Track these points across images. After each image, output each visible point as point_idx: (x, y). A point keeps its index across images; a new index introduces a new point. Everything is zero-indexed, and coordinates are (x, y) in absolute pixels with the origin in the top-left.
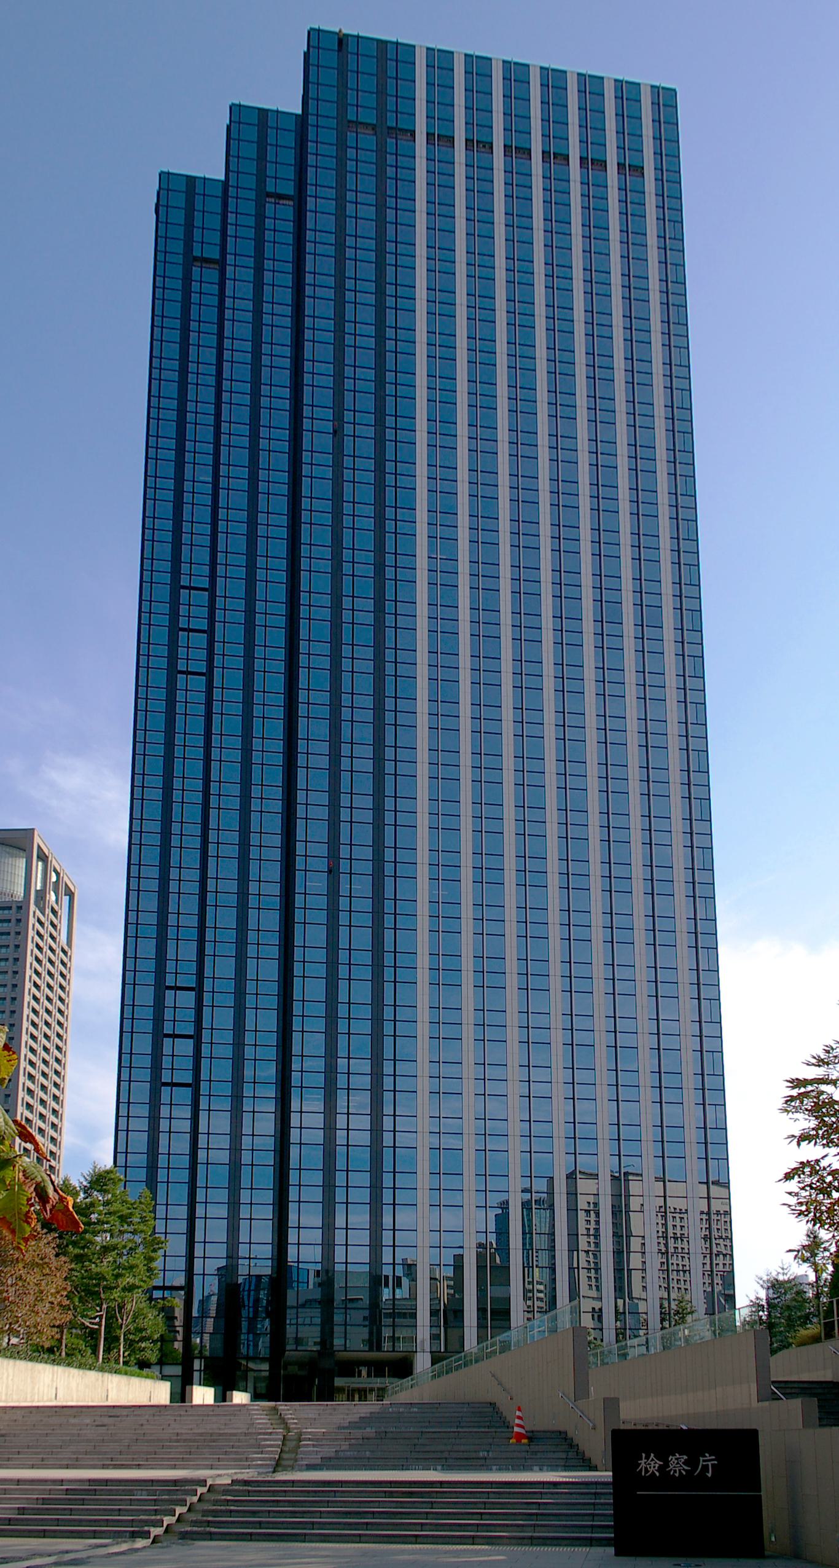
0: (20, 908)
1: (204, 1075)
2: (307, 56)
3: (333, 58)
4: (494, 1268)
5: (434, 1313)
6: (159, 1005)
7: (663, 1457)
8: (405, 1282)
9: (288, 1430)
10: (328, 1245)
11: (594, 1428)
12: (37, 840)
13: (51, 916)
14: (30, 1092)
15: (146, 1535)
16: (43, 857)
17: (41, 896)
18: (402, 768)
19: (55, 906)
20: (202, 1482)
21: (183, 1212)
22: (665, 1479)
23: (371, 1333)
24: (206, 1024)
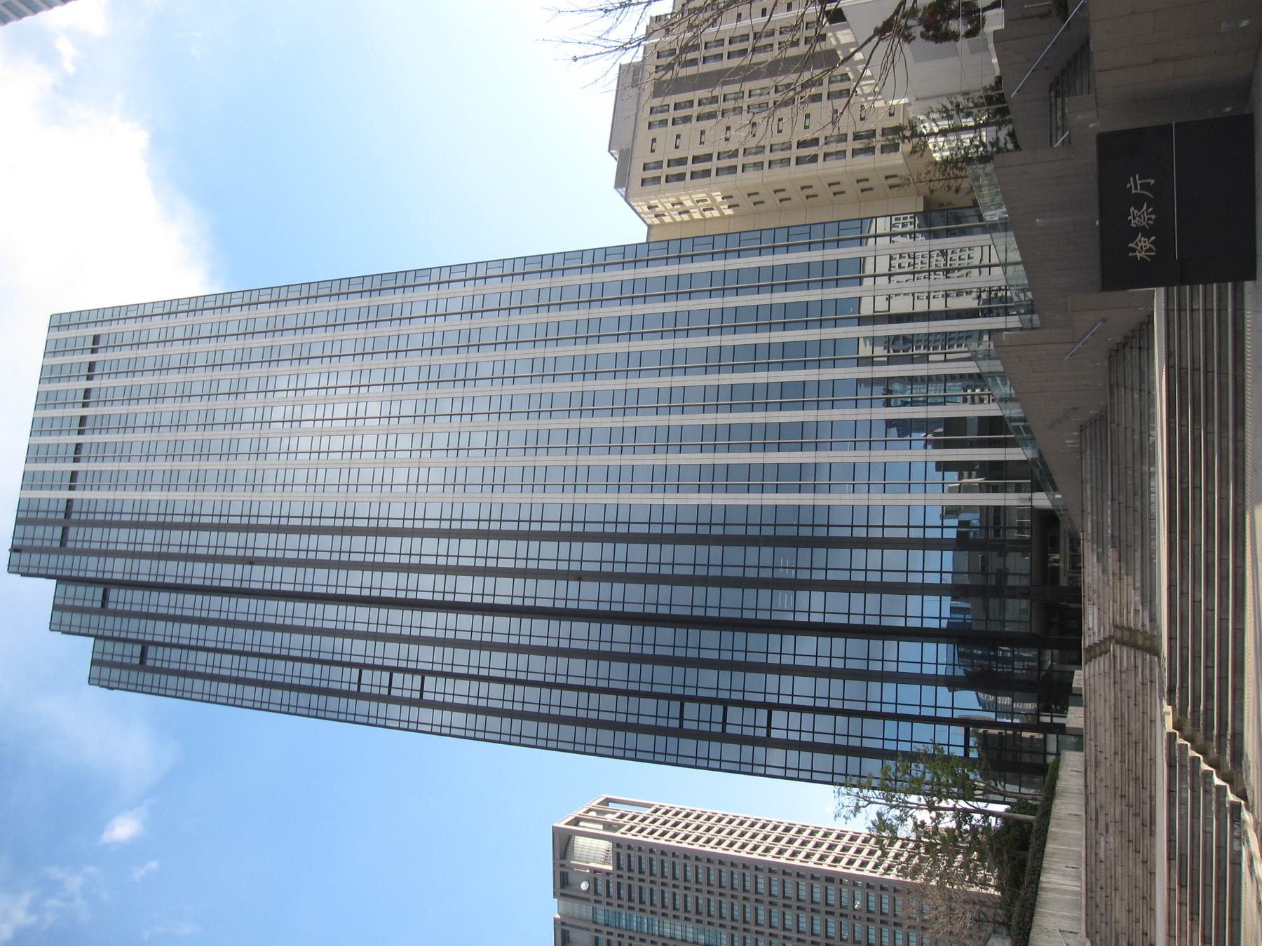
0: (618, 846)
1: (760, 698)
2: (23, 575)
3: (25, 559)
4: (951, 432)
5: (995, 489)
6: (697, 735)
7: (1133, 233)
8: (964, 517)
9: (1111, 637)
10: (924, 589)
11: (1103, 320)
12: (562, 825)
13: (626, 819)
14: (781, 852)
15: (1236, 808)
16: (576, 821)
17: (608, 826)
18: (718, 518)
19: (618, 814)
20: (1171, 737)
21: (891, 725)
22: (1158, 230)
23: (1015, 550)
24: (713, 694)
